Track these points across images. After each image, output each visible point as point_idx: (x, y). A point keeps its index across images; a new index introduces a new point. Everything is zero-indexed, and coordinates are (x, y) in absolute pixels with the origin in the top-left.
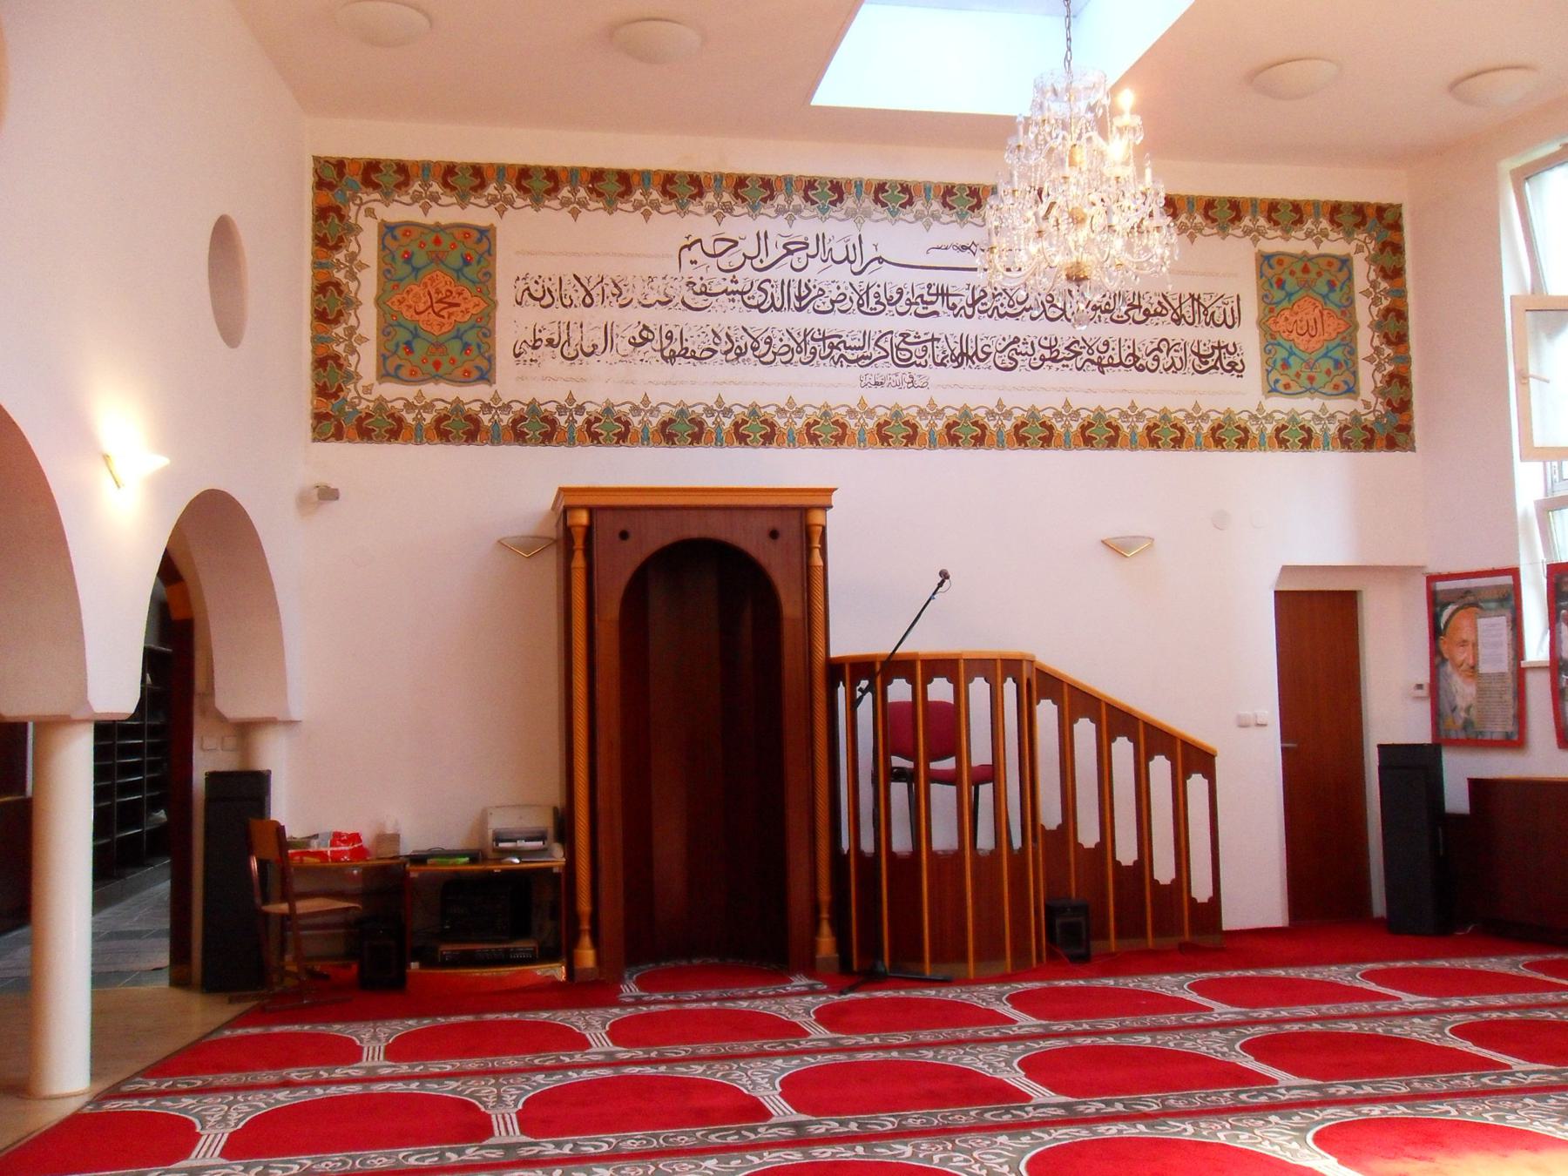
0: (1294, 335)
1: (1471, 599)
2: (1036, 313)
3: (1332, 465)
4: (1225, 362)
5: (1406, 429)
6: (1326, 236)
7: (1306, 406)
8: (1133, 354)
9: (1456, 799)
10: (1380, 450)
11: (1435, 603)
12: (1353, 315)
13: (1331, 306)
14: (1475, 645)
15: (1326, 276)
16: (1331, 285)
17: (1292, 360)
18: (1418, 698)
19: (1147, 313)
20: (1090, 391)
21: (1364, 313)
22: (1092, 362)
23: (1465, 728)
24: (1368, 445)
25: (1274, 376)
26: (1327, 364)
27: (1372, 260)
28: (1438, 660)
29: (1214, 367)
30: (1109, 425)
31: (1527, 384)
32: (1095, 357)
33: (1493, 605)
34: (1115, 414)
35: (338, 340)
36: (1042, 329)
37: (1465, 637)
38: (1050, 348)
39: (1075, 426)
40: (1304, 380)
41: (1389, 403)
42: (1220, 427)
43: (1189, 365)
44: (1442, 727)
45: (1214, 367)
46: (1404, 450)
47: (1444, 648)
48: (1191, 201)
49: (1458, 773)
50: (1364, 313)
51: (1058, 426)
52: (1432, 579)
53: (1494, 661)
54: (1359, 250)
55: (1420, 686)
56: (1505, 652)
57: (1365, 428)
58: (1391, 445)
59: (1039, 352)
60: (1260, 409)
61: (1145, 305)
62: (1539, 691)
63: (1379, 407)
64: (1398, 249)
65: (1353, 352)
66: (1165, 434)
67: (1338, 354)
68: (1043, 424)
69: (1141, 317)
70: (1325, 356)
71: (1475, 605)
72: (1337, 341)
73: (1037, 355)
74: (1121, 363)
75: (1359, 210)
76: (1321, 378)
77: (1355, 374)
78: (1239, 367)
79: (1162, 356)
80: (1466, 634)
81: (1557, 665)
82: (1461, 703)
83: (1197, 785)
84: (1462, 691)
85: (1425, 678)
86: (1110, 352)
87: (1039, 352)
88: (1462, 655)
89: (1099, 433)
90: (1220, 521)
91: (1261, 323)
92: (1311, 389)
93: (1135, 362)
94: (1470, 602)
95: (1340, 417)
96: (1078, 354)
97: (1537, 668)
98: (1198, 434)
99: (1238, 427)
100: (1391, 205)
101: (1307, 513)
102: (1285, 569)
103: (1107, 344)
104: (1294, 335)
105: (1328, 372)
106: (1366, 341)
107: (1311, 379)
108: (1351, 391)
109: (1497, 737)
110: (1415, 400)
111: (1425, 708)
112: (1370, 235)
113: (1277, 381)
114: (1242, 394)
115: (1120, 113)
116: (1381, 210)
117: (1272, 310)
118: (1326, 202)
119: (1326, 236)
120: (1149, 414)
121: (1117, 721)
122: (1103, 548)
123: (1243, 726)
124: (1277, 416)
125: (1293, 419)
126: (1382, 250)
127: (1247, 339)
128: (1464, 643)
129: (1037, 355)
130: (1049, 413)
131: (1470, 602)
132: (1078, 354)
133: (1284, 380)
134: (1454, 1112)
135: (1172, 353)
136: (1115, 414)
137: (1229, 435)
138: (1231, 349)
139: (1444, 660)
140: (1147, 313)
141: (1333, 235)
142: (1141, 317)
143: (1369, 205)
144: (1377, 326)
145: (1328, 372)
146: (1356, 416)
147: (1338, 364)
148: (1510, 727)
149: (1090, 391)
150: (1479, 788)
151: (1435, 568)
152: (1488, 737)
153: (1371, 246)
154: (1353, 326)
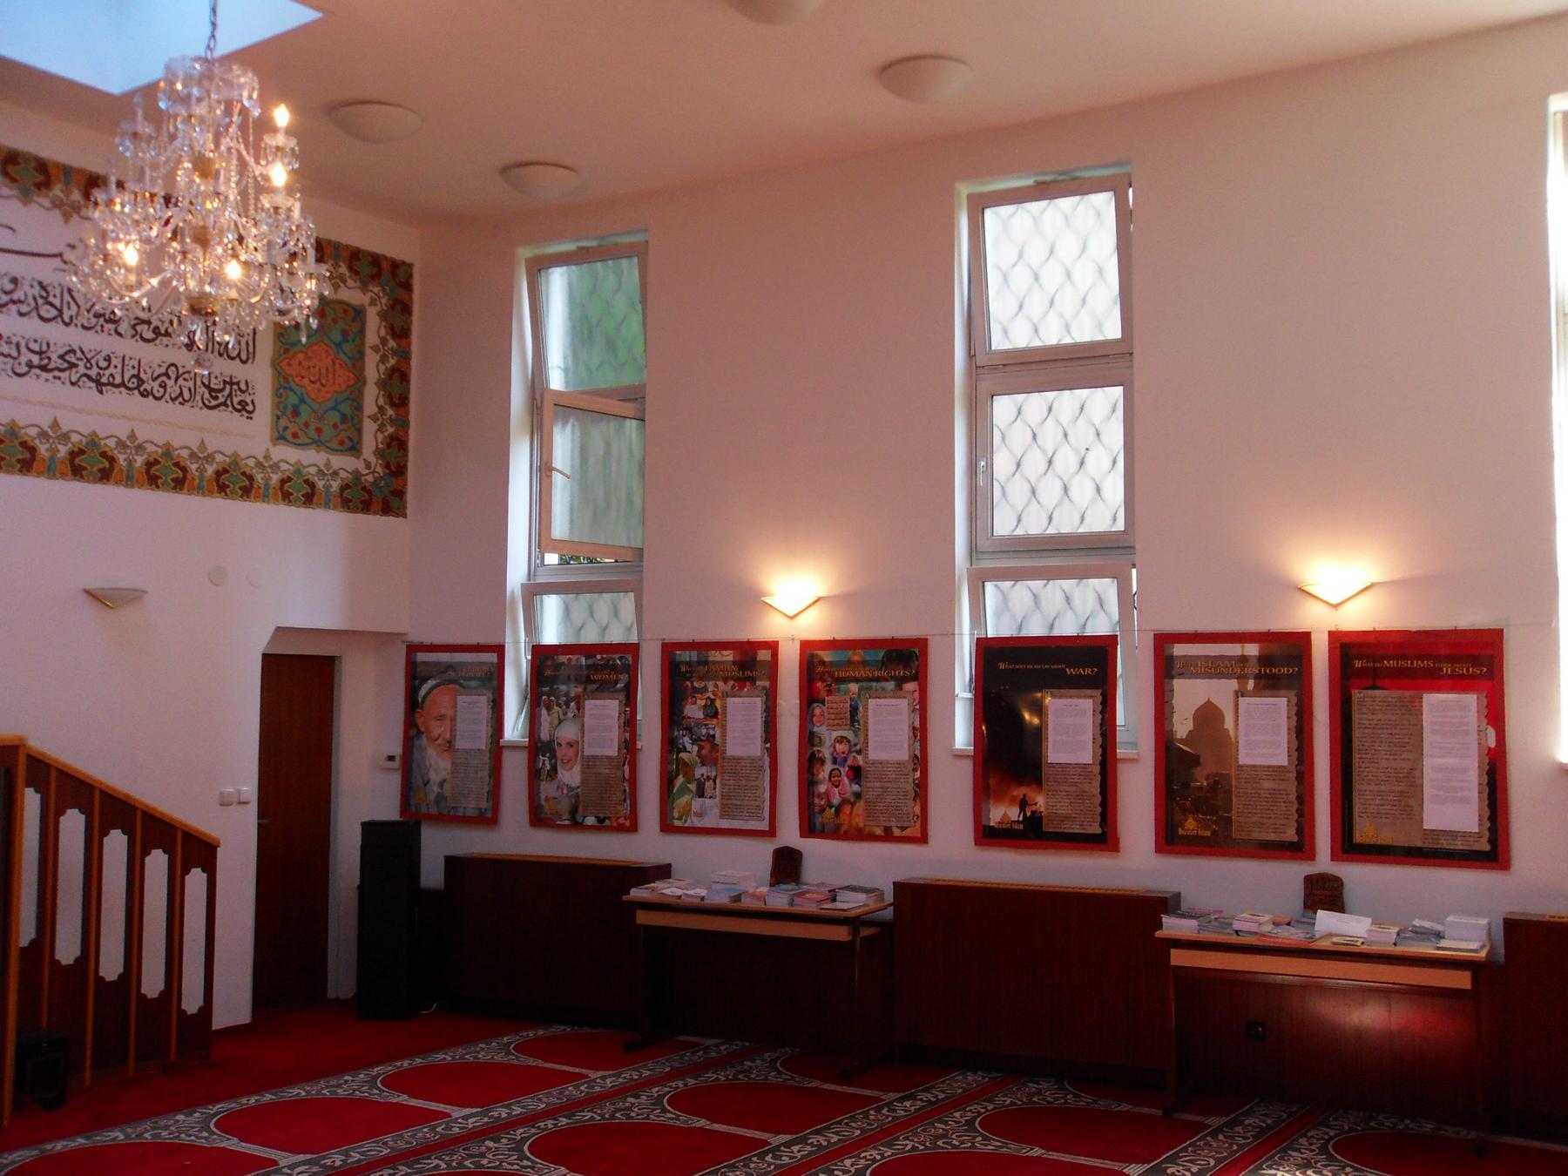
0: (306, 381)
1: (452, 674)
2: (24, 308)
3: (330, 524)
4: (236, 400)
5: (400, 494)
6: (344, 282)
7: (311, 459)
8: (137, 376)
9: (432, 874)
10: (375, 513)
11: (414, 676)
12: (363, 368)
13: (342, 356)
14: (453, 719)
15: (342, 324)
16: (345, 334)
17: (303, 408)
18: (388, 769)
19: (156, 331)
20: (81, 411)
21: (373, 369)
22: (90, 378)
23: (437, 802)
24: (366, 507)
25: (284, 422)
26: (335, 417)
27: (383, 316)
28: (413, 732)
29: (224, 404)
30: (104, 454)
31: (550, 477)
32: (93, 373)
33: (474, 683)
34: (112, 443)
35: (54, 451)
36: (31, 329)
37: (443, 711)
38: (40, 353)
39: (63, 451)
40: (312, 432)
41: (387, 466)
42: (225, 471)
43: (198, 398)
44: (413, 802)
45: (224, 404)
46: (397, 515)
47: (420, 721)
48: (337, 246)
49: (438, 846)
50: (373, 369)
51: (43, 449)
52: (413, 649)
53: (472, 737)
54: (373, 303)
55: (391, 758)
56: (484, 730)
57: (364, 489)
58: (387, 510)
59: (26, 356)
60: (267, 457)
61: (155, 323)
62: (515, 771)
63: (379, 469)
64: (406, 309)
65: (359, 407)
66: (165, 473)
67: (346, 408)
68: (24, 444)
69: (150, 335)
70: (333, 408)
71: (455, 681)
72: (346, 394)
73: (23, 360)
74: (123, 384)
75: (376, 260)
76: (328, 432)
77: (359, 431)
78: (250, 408)
79: (170, 383)
80: (444, 707)
81: (537, 746)
82: (435, 777)
83: (196, 880)
84: (437, 766)
85: (397, 750)
86: (112, 370)
87: (26, 356)
88: (438, 729)
89: (90, 463)
90: (217, 577)
91: (275, 364)
92: (317, 443)
93: (137, 385)
94: (452, 678)
95: (343, 474)
96: (73, 366)
97: (514, 747)
98: (202, 477)
99: (244, 474)
100: (404, 263)
101: (293, 573)
102: (278, 629)
103: (108, 359)
104: (306, 381)
105: (335, 426)
106: (372, 398)
107: (319, 430)
108: (354, 449)
109: (470, 813)
110: (410, 465)
111: (395, 780)
112: (383, 290)
113: (286, 428)
114: (249, 437)
115: (274, 130)
116: (396, 265)
117: (286, 351)
118: (347, 247)
119: (344, 282)
120: (150, 448)
121: (110, 810)
122: (85, 597)
123: (225, 803)
124: (284, 466)
125: (298, 472)
126: (392, 307)
127: (260, 377)
128: (441, 717)
129: (23, 360)
130: (33, 432)
131: (452, 678)
132: (73, 366)
133: (292, 428)
134: (121, 1137)
135: (181, 381)
136: (112, 443)
137: (233, 481)
138: (243, 387)
139: (419, 733)
140: (156, 331)
141: (350, 282)
142: (150, 335)
143: (386, 258)
144: (382, 385)
145: (335, 426)
146: (357, 475)
147: (344, 419)
148: (484, 804)
149: (81, 411)
150: (452, 863)
151: (418, 637)
152: (460, 813)
153: (384, 301)
154: (361, 380)
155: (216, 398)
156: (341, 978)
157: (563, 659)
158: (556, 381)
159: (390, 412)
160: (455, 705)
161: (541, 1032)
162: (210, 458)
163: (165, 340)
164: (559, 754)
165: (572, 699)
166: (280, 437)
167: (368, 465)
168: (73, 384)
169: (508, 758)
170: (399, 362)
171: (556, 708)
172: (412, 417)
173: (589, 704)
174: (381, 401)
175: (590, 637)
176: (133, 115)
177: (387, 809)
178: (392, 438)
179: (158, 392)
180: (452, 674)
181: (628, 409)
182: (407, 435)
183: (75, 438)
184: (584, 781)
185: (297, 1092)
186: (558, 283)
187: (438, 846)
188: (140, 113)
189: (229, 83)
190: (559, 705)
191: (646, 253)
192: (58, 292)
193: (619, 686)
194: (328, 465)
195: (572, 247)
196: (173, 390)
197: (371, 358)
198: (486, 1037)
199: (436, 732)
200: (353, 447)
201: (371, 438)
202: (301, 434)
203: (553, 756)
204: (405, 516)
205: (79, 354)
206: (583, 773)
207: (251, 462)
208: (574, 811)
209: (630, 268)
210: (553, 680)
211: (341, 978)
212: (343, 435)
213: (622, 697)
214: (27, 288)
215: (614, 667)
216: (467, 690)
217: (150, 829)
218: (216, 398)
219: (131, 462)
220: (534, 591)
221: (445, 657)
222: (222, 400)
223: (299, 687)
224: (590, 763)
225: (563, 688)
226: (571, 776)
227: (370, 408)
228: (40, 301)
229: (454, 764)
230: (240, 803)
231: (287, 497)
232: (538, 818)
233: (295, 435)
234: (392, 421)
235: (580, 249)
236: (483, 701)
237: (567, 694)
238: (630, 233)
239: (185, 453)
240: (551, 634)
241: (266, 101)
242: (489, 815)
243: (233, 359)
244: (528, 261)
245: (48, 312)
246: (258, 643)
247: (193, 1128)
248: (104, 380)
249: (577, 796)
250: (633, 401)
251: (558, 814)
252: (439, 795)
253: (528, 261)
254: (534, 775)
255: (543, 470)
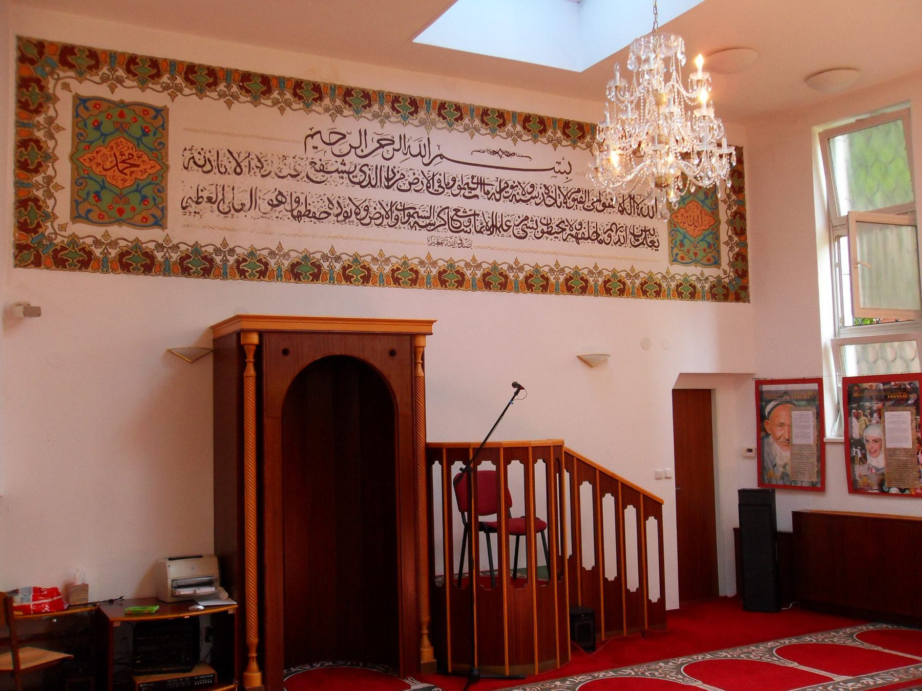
1: (787, 398)
2: (538, 201)
3: (706, 308)
4: (648, 241)
5: (745, 288)
7: (693, 271)
8: (596, 232)
9: (784, 523)
11: (761, 399)
13: (706, 208)
14: (790, 426)
18: (750, 457)
19: (604, 205)
24: (726, 298)
25: (676, 251)
26: (704, 245)
28: (763, 434)
32: (574, 233)
33: (803, 403)
34: (586, 271)
35: (557, 279)
37: (782, 421)
38: (547, 225)
40: (691, 255)
41: (736, 272)
42: (646, 283)
43: (628, 241)
44: (766, 477)
46: (744, 302)
47: (767, 428)
49: (786, 508)
52: (759, 383)
53: (804, 435)
55: (750, 450)
56: (812, 433)
57: (724, 287)
58: (738, 299)
62: (835, 459)
63: (732, 274)
65: (717, 238)
66: (614, 287)
70: (703, 240)
71: (790, 402)
72: (710, 230)
73: (539, 229)
74: (589, 238)
76: (701, 254)
77: (719, 252)
78: (656, 244)
79: (613, 234)
81: (849, 442)
82: (779, 462)
84: (780, 455)
85: (753, 445)
86: (583, 230)
87: (541, 227)
89: (576, 284)
90: (645, 344)
92: (695, 262)
93: (596, 237)
95: (711, 279)
96: (564, 230)
97: (833, 443)
99: (656, 283)
101: (688, 340)
103: (581, 224)
106: (724, 231)
107: (696, 254)
108: (716, 263)
109: (804, 485)
110: (750, 270)
111: (753, 465)
113: (677, 255)
114: (656, 262)
121: (606, 483)
122: (579, 362)
125: (686, 280)
127: (661, 227)
128: (782, 425)
129: (539, 229)
131: (786, 399)
132: (564, 230)
134: (633, 673)
135: (619, 233)
136: (586, 271)
137: (650, 289)
138: (652, 232)
139: (768, 435)
140: (604, 205)
144: (730, 223)
145: (705, 250)
147: (710, 246)
150: (798, 517)
154: (718, 222)
155: (638, 240)
156: (727, 585)
157: (866, 385)
158: (844, 208)
159: (736, 239)
160: (791, 417)
161: (871, 628)
162: (637, 276)
163: (609, 210)
164: (867, 446)
165: (875, 412)
166: (674, 260)
167: (725, 272)
168: (564, 240)
169: (829, 450)
170: (738, 208)
171: (863, 418)
172: (749, 241)
173: (888, 415)
174: (730, 233)
175: (881, 370)
176: (614, 77)
177: (752, 483)
178: (738, 254)
179: (607, 240)
180: (787, 398)
181: (905, 219)
182: (746, 252)
183: (567, 270)
184: (887, 465)
185: (724, 654)
186: (840, 145)
187: (786, 508)
188: (618, 75)
189: (668, 47)
190: (866, 416)
191: (909, 115)
192: (553, 189)
193: (910, 402)
194: (702, 274)
195: (852, 120)
196: (615, 238)
197: (722, 207)
198: (836, 627)
199: (779, 434)
200: (716, 262)
201: (726, 255)
202: (686, 257)
203: (863, 448)
204: (749, 302)
205: (566, 223)
206: (886, 459)
207: (659, 276)
208: (881, 484)
209: (896, 130)
210: (860, 399)
211: (727, 585)
212: (709, 255)
213: (913, 409)
214: (538, 189)
215: (905, 390)
216: (797, 407)
217: (628, 494)
218: (638, 240)
219: (596, 282)
220: (839, 344)
221: (782, 387)
222: (641, 241)
223: (693, 408)
224: (891, 453)
225: (867, 404)
226: (878, 461)
227: (724, 237)
228: (546, 196)
229: (792, 454)
230: (667, 478)
231: (680, 295)
232: (854, 488)
233: (682, 258)
234: (737, 244)
235: (857, 121)
236: (809, 415)
237: (870, 408)
238: (894, 105)
239: (624, 274)
240: (852, 371)
241: (690, 54)
242: (819, 486)
243: (645, 216)
244: (819, 134)
245: (550, 201)
246: (670, 383)
247: (667, 670)
248: (579, 236)
249: (883, 474)
250: (906, 214)
251: (869, 486)
252: (783, 473)
253: (819, 134)
254: (850, 461)
255: (836, 265)
